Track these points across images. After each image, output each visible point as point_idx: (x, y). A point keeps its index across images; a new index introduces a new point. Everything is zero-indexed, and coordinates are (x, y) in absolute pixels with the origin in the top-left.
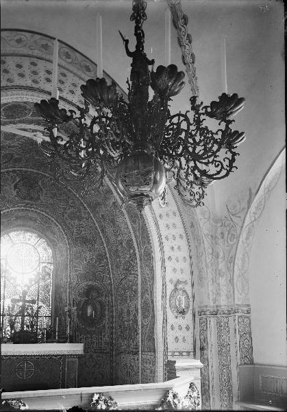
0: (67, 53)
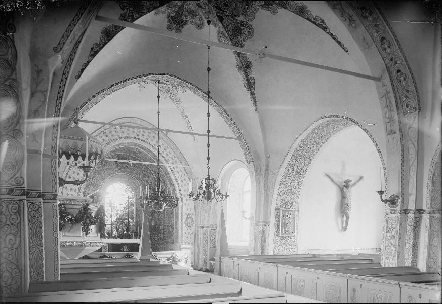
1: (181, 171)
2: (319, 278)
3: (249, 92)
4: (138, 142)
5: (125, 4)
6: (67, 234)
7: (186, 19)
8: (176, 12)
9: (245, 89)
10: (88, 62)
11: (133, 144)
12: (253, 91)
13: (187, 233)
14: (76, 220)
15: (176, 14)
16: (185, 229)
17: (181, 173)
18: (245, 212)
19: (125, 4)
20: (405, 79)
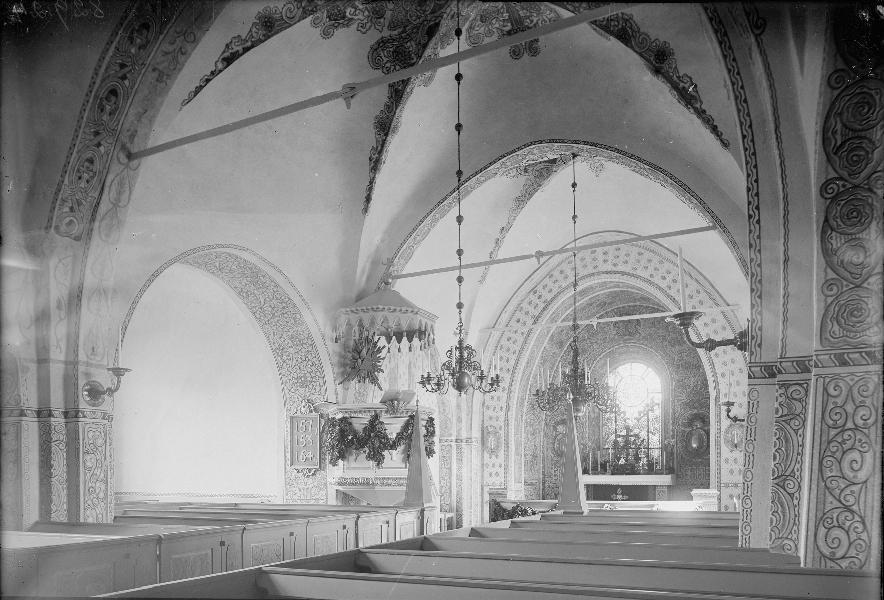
0: (330, 462)
1: (714, 321)
2: (127, 556)
3: (692, 111)
4: (632, 281)
5: (388, 65)
6: (353, 464)
7: (532, 21)
8: (510, 19)
9: (681, 108)
10: (372, 182)
11: (612, 285)
12: (698, 106)
13: (497, 464)
14: (360, 442)
15: (512, 24)
16: (725, 450)
17: (715, 326)
18: (733, 404)
19: (388, 65)
20: (140, 48)
